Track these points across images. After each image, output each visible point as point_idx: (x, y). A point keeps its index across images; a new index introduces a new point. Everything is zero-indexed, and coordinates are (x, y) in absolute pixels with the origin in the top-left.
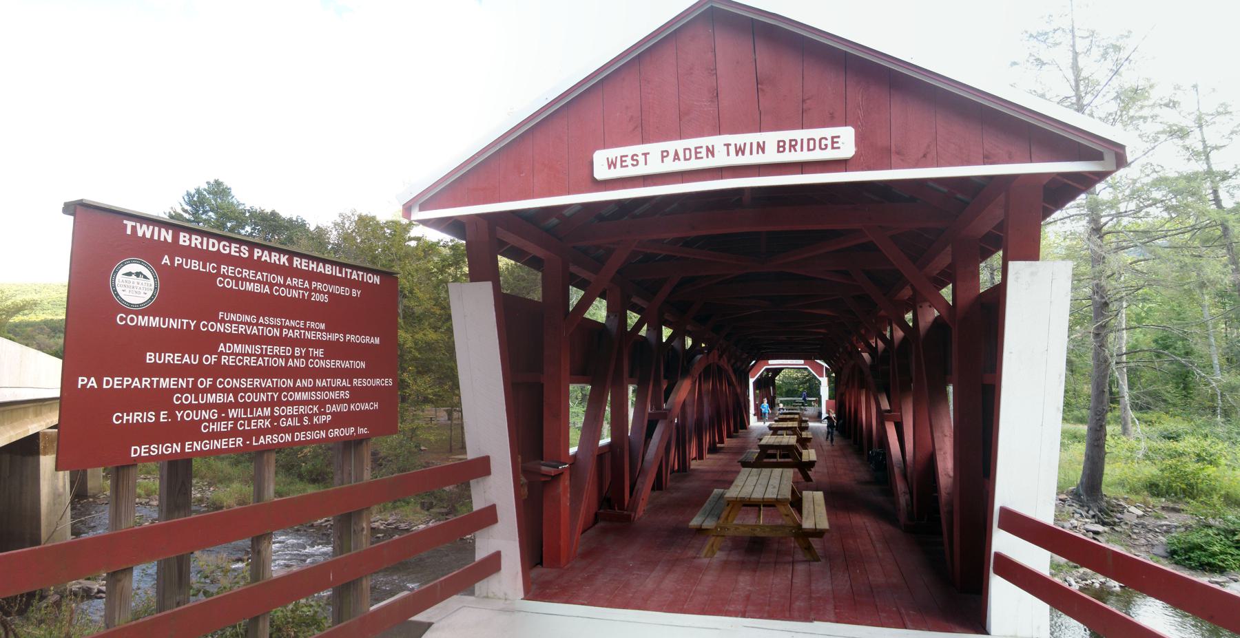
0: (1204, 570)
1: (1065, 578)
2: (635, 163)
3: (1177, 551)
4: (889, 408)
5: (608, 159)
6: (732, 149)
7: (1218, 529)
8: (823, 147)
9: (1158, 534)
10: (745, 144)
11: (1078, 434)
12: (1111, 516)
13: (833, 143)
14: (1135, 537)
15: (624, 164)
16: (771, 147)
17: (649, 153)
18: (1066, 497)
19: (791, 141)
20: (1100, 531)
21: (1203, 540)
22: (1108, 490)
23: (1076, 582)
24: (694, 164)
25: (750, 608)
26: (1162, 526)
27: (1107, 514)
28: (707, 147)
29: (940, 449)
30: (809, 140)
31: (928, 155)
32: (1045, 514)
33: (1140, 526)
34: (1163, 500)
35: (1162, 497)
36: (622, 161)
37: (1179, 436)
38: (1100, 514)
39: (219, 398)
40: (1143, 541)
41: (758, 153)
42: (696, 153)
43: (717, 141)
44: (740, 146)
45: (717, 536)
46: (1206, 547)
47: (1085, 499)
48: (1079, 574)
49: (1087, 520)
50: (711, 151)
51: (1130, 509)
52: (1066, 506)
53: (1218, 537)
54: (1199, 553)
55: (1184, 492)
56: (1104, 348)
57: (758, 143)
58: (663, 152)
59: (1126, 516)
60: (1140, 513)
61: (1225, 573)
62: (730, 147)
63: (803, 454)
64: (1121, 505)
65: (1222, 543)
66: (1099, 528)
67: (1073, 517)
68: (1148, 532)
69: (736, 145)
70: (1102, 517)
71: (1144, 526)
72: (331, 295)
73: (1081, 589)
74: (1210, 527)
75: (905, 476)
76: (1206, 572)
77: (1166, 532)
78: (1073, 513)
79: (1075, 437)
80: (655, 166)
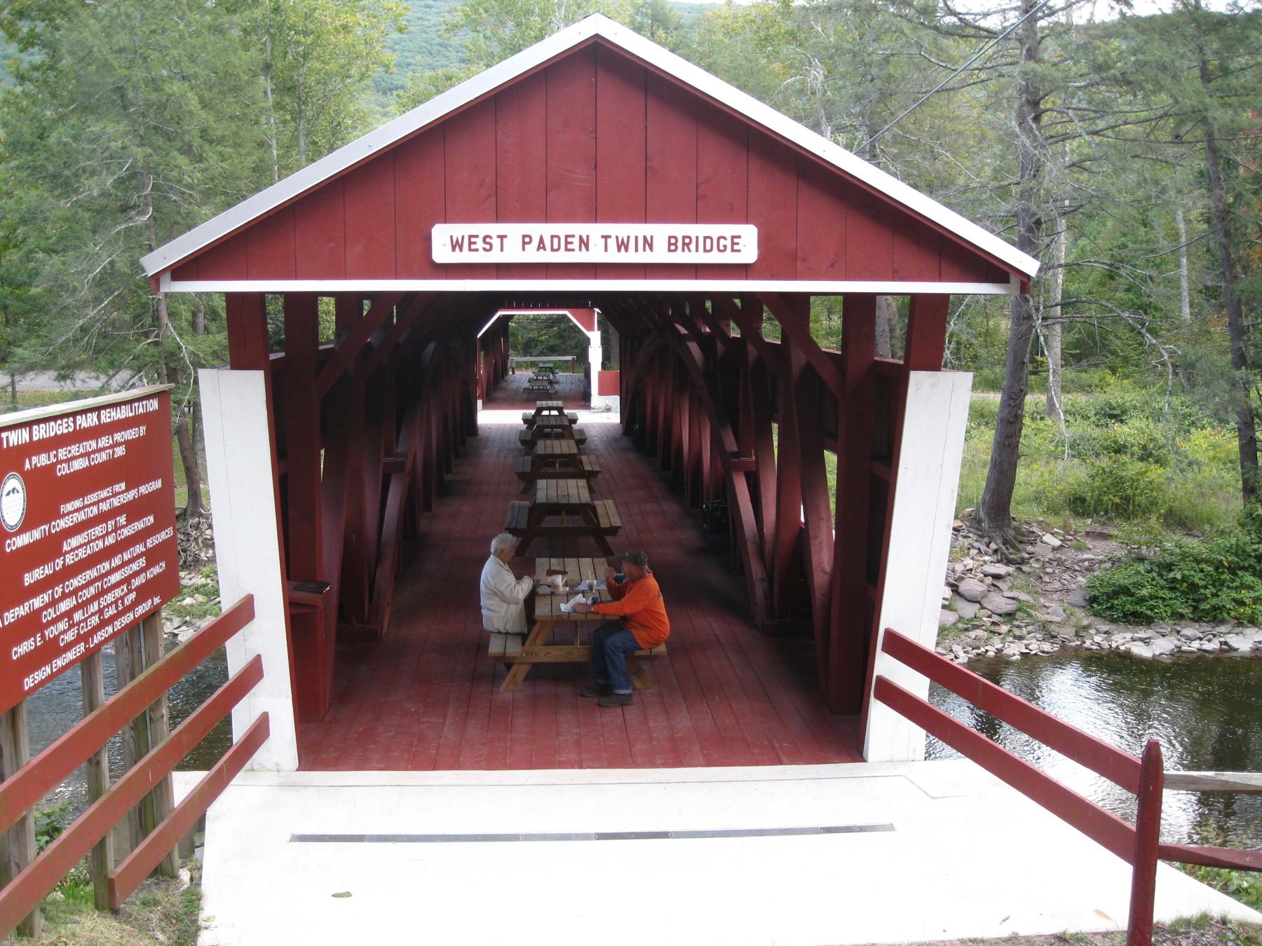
0: (1128, 622)
1: (951, 647)
2: (488, 247)
3: (1098, 597)
4: (735, 449)
5: (451, 237)
6: (612, 243)
7: (1152, 563)
8: (722, 248)
9: (1078, 573)
10: (628, 237)
11: (986, 412)
12: (1019, 550)
13: (733, 244)
14: (1046, 579)
15: (473, 247)
16: (661, 244)
17: (505, 236)
18: (961, 524)
19: (684, 237)
20: (1003, 573)
21: (1131, 581)
22: (1019, 511)
23: (965, 652)
24: (562, 257)
25: (584, 756)
26: (1083, 561)
27: (1014, 547)
28: (581, 237)
29: (816, 538)
30: (705, 238)
31: (836, 265)
32: (926, 639)
33: (1055, 563)
34: (1089, 521)
35: (1088, 518)
36: (470, 243)
37: (1124, 412)
38: (1004, 548)
39: (64, 606)
40: (1057, 585)
41: (644, 250)
42: (567, 243)
43: (594, 231)
44: (623, 240)
45: (522, 664)
46: (1133, 590)
47: (987, 526)
48: (969, 640)
49: (987, 558)
50: (584, 243)
51: (1045, 539)
52: (960, 538)
53: (1150, 575)
54: (1124, 599)
55: (1117, 508)
56: (1028, 296)
57: (645, 238)
58: (524, 236)
59: (1037, 549)
60: (1057, 543)
61: (1152, 625)
62: (609, 240)
63: (597, 507)
64: (1033, 532)
65: (1154, 583)
66: (1001, 569)
67: (968, 554)
68: (1065, 571)
69: (617, 237)
70: (1006, 552)
71: (1060, 563)
72: (128, 444)
73: (970, 664)
74: (1141, 559)
75: (761, 555)
76: (1131, 624)
77: (1087, 570)
78: (969, 549)
79: (982, 416)
80: (513, 254)
